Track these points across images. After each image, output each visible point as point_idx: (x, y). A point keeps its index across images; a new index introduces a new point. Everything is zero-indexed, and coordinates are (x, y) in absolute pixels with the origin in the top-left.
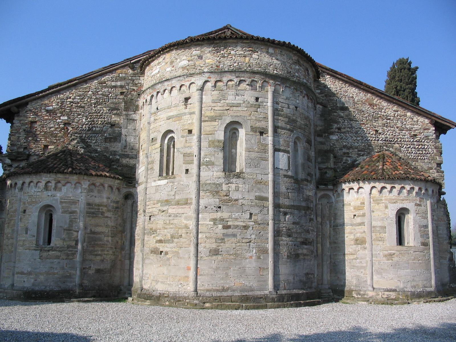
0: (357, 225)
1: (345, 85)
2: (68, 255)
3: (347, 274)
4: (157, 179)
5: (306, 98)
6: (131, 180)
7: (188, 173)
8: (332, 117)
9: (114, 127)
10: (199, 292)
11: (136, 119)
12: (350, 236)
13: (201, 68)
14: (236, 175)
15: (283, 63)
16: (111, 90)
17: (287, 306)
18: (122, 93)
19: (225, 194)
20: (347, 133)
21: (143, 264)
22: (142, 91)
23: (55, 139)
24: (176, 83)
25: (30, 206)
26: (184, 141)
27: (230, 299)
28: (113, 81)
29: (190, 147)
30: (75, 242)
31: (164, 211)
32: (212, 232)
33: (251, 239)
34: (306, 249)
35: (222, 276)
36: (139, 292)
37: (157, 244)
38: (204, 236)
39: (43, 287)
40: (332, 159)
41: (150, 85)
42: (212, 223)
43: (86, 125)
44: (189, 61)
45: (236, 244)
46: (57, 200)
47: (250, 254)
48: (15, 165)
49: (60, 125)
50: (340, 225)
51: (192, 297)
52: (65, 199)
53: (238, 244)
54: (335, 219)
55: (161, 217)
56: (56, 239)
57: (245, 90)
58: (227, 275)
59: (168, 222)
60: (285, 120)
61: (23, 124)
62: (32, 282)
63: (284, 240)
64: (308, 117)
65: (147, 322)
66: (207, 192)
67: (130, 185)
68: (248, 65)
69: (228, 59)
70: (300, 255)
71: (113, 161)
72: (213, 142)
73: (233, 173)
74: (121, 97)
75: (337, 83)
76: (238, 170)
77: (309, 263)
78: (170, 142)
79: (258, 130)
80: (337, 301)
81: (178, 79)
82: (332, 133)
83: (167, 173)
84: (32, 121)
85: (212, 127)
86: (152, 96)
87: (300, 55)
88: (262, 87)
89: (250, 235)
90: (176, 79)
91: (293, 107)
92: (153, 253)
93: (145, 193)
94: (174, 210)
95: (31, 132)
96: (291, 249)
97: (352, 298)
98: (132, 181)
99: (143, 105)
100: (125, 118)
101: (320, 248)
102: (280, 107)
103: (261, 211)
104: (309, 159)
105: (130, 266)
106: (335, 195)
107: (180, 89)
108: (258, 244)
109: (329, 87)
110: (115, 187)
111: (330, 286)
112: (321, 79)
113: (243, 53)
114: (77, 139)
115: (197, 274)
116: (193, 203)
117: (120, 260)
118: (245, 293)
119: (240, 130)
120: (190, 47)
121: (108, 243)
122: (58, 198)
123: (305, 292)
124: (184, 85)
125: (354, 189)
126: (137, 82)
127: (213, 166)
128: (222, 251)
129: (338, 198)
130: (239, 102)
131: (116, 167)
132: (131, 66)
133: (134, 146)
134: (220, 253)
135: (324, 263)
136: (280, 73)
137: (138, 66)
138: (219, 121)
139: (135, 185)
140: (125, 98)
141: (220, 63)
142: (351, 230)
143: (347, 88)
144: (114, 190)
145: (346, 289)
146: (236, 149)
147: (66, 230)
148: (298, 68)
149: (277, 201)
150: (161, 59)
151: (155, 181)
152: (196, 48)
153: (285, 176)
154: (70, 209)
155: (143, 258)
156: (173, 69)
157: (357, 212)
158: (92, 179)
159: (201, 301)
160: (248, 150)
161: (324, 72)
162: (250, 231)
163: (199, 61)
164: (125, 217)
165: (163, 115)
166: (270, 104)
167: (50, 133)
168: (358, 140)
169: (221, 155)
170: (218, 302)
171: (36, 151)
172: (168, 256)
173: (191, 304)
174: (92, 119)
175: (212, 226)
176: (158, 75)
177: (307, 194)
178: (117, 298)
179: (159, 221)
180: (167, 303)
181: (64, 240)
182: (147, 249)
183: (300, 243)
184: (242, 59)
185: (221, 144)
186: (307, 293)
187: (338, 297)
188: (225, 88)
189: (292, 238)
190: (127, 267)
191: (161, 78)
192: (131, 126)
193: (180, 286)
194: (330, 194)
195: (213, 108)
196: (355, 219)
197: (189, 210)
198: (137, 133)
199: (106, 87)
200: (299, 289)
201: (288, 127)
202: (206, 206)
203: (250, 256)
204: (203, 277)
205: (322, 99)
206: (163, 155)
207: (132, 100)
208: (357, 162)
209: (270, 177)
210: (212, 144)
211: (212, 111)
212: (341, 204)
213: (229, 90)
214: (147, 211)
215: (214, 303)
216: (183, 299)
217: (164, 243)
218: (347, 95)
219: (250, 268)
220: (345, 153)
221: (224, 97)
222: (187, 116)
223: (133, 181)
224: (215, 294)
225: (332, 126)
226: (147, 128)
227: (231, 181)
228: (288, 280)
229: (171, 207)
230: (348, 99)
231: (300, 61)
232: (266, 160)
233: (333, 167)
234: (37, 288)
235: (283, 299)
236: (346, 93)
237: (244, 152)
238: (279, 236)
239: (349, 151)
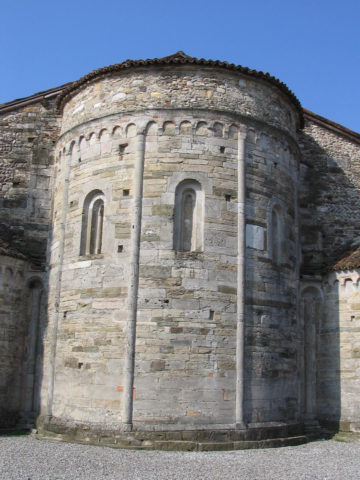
0: (357, 330)
1: (337, 138)
3: (342, 399)
4: (76, 259)
5: (288, 152)
6: (39, 260)
7: (121, 251)
8: (320, 181)
9: (19, 186)
10: (135, 424)
11: (49, 176)
12: (346, 346)
13: (144, 104)
14: (191, 256)
15: (259, 102)
16: (16, 134)
17: (261, 446)
18: (30, 140)
19: (175, 282)
20: (341, 203)
21: (53, 381)
22: (58, 138)
24: (108, 124)
26: (117, 206)
27: (180, 435)
28: (18, 123)
29: (126, 214)
31: (85, 305)
32: (155, 336)
33: (212, 348)
34: (287, 363)
35: (168, 401)
36: (46, 421)
37: (75, 353)
38: (144, 343)
40: (320, 240)
41: (70, 127)
42: (155, 324)
44: (127, 94)
45: (189, 354)
47: (209, 370)
50: (332, 331)
51: (125, 431)
53: (193, 355)
54: (324, 321)
55: (81, 314)
57: (206, 135)
58: (176, 399)
59: (91, 321)
60: (261, 181)
63: (259, 350)
64: (290, 177)
65: (58, 472)
66: (148, 280)
67: (38, 267)
68: (210, 101)
69: (183, 92)
70: (279, 372)
71: (15, 234)
72: (159, 207)
73: (187, 252)
74: (29, 145)
75: (326, 136)
76: (193, 249)
77: (291, 383)
78: (97, 208)
79: (223, 193)
80: (328, 437)
81: (111, 119)
82: (320, 204)
83: (92, 252)
85: (158, 186)
86: (73, 143)
87: (281, 92)
88: (229, 133)
89: (210, 342)
90: (108, 118)
91: (272, 163)
92: (68, 365)
93: (58, 280)
94: (100, 304)
96: (268, 363)
97: (348, 434)
98: (40, 262)
99: (60, 156)
100: (33, 174)
101: (303, 363)
102: (254, 162)
103: (226, 308)
104: (291, 237)
105: (34, 383)
106: (324, 288)
107: (113, 133)
108: (221, 355)
109: (316, 140)
110: (16, 269)
111: (316, 415)
112: (306, 130)
113: (204, 85)
115: (132, 398)
116: (129, 295)
117: (21, 375)
118: (202, 426)
119: (198, 192)
120: (129, 75)
121: (4, 350)
123: (285, 424)
124: (119, 127)
125: (353, 280)
126: (52, 125)
127: (159, 242)
128: (169, 365)
129: (329, 292)
130: (197, 152)
131: (19, 242)
132: (44, 102)
133: (45, 213)
134: (166, 368)
135: (309, 383)
136: (255, 114)
137: (53, 103)
138: (169, 178)
139: (44, 267)
140: (35, 146)
141: (170, 97)
142: (348, 337)
143: (340, 143)
144: (15, 274)
145: (341, 420)
146: (191, 218)
148: (278, 109)
149: (248, 294)
150: (86, 92)
151: (73, 262)
152: (138, 76)
153: (261, 259)
155: (54, 371)
156: (104, 104)
157: (356, 312)
159: (137, 438)
160: (209, 221)
161: (310, 120)
162: (210, 337)
163: (141, 94)
164: (29, 314)
165: (87, 169)
166: (240, 156)
168: (355, 214)
169: (170, 226)
170: (163, 439)
172: (89, 370)
173: (123, 442)
175: (155, 329)
176: (83, 114)
177: (289, 285)
178: (14, 429)
179: (79, 319)
180: (87, 439)
182: (59, 360)
183: (279, 354)
184: (202, 93)
185: (171, 211)
186: (288, 427)
187: (328, 432)
188: (177, 132)
189: (268, 347)
190: (30, 384)
191: (85, 118)
192: (42, 184)
193: (107, 415)
194: (317, 287)
195: (161, 160)
196: (354, 322)
197: (123, 304)
198: (50, 195)
199: (8, 130)
200: (277, 421)
201: (265, 190)
202: (147, 299)
203: (210, 373)
204: (141, 402)
205: (306, 157)
206: (86, 226)
207: (45, 149)
208: (354, 244)
209: (240, 259)
210: (158, 210)
211: (159, 164)
212: (333, 301)
213: (183, 135)
214: (61, 304)
215: (156, 441)
216: (111, 434)
217: (85, 351)
218: (341, 152)
219: (209, 390)
220: (337, 231)
221: (176, 145)
222: (122, 171)
223: (43, 262)
224: (158, 427)
225: (320, 193)
226: (64, 189)
227: (184, 264)
228: (263, 408)
229: (97, 299)
230: (342, 158)
231: (281, 100)
232: (234, 234)
233: (322, 250)
235: (256, 435)
236: (338, 150)
237: (202, 224)
238: (251, 344)
239: (342, 229)
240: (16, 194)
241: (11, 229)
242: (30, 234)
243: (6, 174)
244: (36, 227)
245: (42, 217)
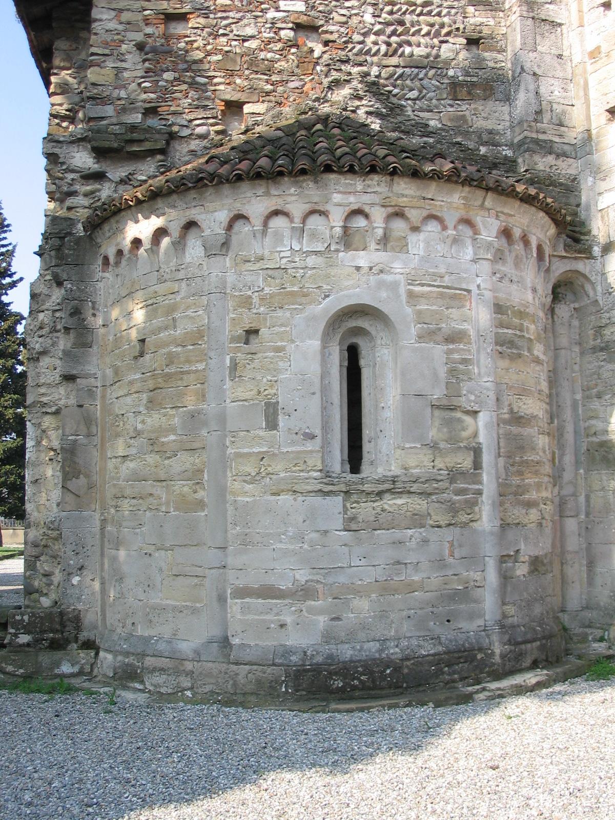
2: (453, 509)
11: (559, 21)
23: (267, 81)
25: (280, 313)
30: (472, 453)
39: (373, 646)
43: (377, 34)
46: (394, 286)
48: (117, 172)
49: (280, 29)
52: (423, 285)
56: (407, 445)
61: (129, 23)
62: (321, 626)
71: (495, 166)
84: (171, 11)
95: (169, 52)
114: (348, 81)
122: (398, 277)
133: (564, 113)
147: (438, 407)
154: (444, 325)
158: (506, 211)
167: (247, 58)
171: (198, 122)
174: (395, 16)
181: (434, 446)
192: (547, 43)
234: (350, 652)
240: (477, 66)
241: (481, 153)
242: (540, 164)
243: (445, 16)
244: (551, 147)
245: (560, 122)
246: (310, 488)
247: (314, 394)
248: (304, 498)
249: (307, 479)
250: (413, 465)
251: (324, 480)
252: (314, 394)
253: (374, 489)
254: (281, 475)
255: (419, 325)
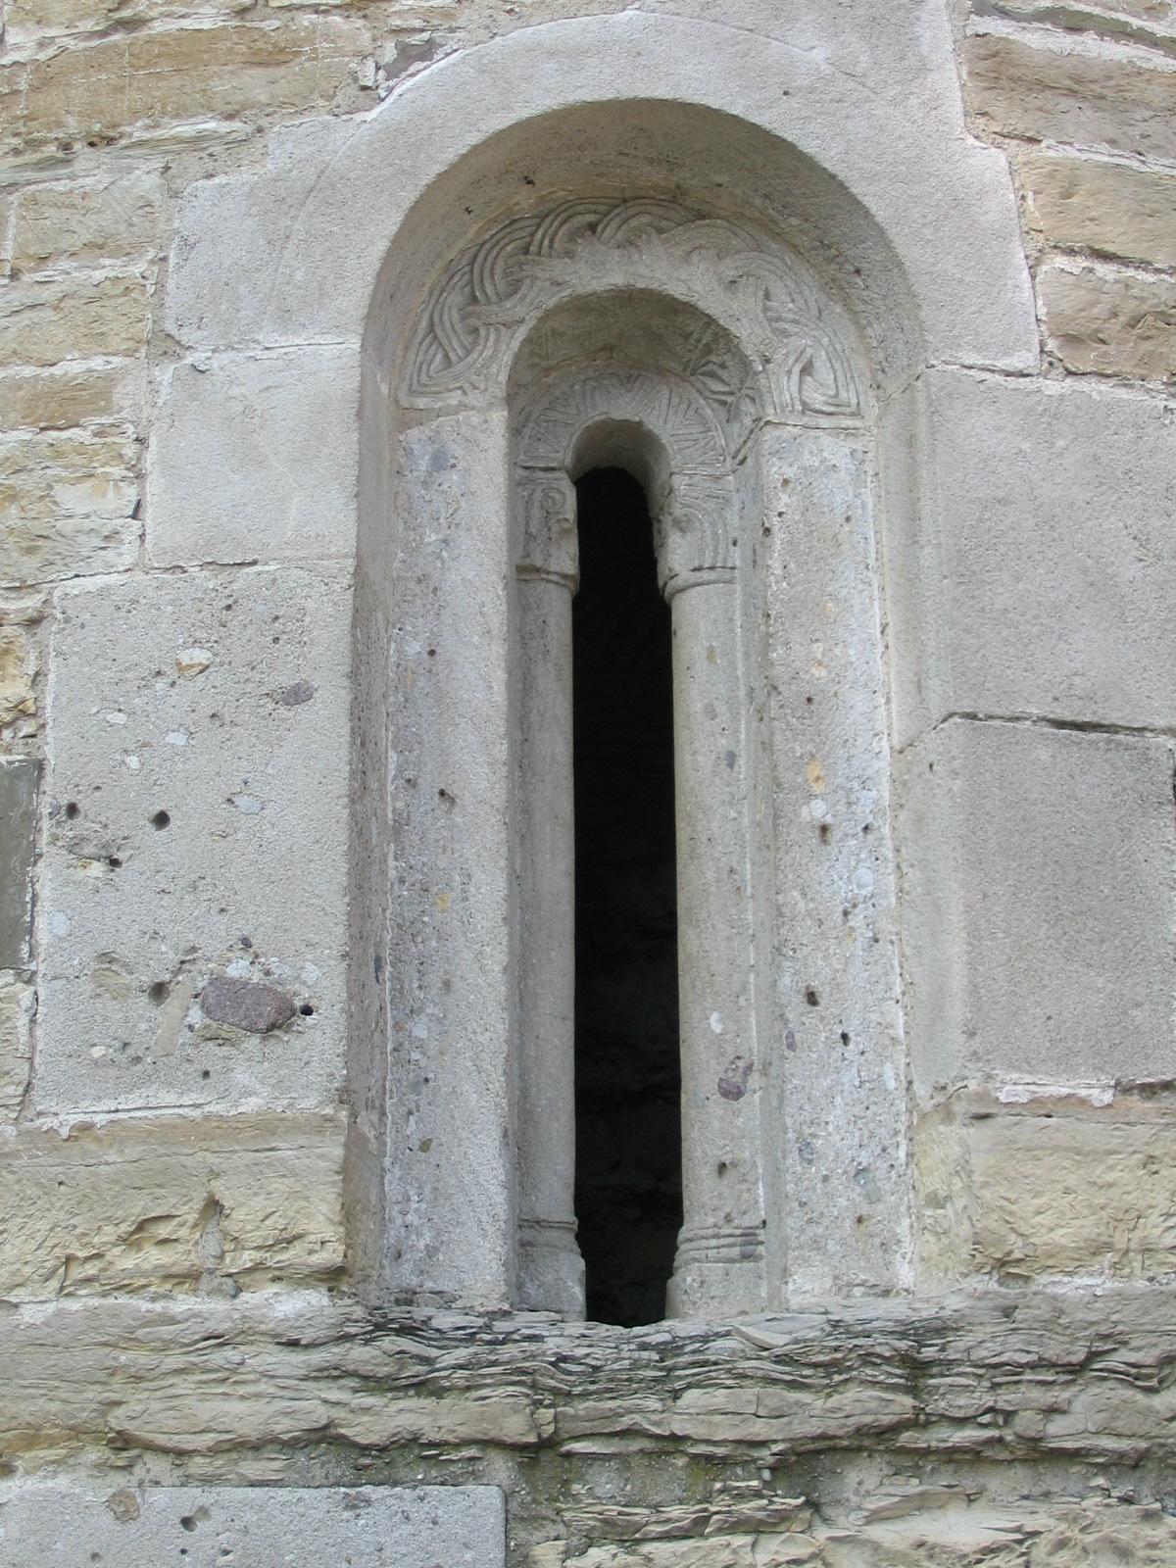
25: (92, 172)
56: (1013, 1089)
246: (243, 1415)
247: (297, 695)
248: (192, 1497)
249: (220, 1340)
250: (1061, 1237)
251: (358, 1355)
252: (297, 695)
253: (759, 1429)
254: (30, 1314)
255: (1061, 261)
